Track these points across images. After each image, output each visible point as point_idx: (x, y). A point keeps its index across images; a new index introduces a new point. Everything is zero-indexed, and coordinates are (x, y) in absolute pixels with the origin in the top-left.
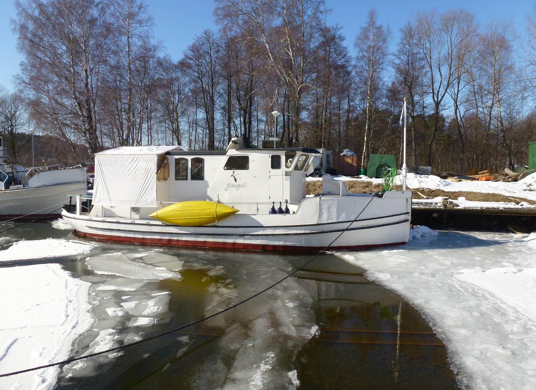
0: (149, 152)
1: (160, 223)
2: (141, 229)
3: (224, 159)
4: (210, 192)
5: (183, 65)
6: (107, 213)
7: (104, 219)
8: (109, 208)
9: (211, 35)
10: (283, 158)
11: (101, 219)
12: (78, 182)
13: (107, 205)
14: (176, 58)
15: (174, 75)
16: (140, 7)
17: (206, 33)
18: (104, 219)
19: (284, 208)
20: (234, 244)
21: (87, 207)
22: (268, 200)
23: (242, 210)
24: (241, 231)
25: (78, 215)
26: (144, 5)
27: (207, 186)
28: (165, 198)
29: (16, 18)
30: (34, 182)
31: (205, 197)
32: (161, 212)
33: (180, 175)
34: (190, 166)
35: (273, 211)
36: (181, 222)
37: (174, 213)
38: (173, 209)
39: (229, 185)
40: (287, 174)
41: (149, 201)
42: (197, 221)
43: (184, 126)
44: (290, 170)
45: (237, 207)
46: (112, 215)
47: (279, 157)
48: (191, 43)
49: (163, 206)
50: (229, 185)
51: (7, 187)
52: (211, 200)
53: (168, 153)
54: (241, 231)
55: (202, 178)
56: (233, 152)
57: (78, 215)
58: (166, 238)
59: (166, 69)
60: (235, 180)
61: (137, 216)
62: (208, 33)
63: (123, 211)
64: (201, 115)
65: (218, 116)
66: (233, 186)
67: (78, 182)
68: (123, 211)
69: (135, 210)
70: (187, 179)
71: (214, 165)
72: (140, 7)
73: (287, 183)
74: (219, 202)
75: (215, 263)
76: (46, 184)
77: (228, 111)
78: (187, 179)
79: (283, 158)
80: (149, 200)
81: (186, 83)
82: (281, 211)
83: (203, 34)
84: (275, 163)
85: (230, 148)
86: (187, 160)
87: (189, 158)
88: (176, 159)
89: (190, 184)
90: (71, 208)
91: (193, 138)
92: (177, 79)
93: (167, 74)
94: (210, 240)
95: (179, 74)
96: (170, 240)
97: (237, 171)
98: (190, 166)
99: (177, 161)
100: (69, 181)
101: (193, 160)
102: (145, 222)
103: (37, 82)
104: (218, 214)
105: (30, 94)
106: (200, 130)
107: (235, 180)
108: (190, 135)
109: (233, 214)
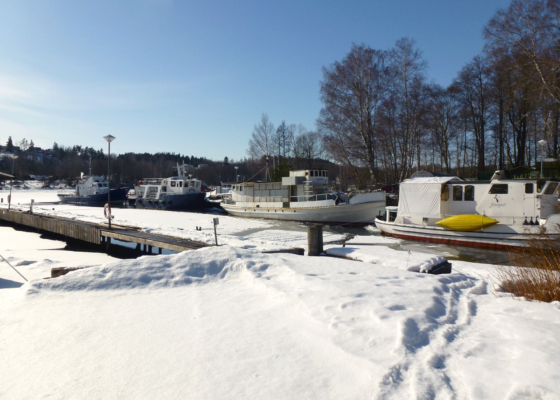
0: (435, 182)
1: (443, 229)
2: (429, 231)
3: (489, 187)
4: (477, 209)
5: (453, 90)
6: (406, 221)
7: (405, 225)
8: (408, 218)
9: (481, 60)
10: (535, 186)
11: (403, 225)
12: (380, 201)
13: (406, 216)
14: (445, 83)
15: (443, 100)
16: (416, 55)
17: (475, 59)
18: (405, 225)
19: (534, 221)
20: (495, 245)
21: (393, 216)
22: (522, 215)
23: (502, 222)
24: (500, 236)
25: (387, 222)
26: (418, 53)
27: (476, 204)
28: (446, 212)
29: (322, 79)
30: (353, 201)
31: (474, 212)
32: (444, 221)
33: (458, 198)
34: (464, 191)
35: (526, 223)
36: (457, 228)
37: (452, 222)
38: (452, 219)
39: (493, 205)
40: (538, 197)
41: (435, 214)
42: (469, 228)
43: (452, 147)
44: (541, 194)
45: (498, 220)
46: (410, 223)
47: (531, 185)
48: (460, 69)
49: (445, 217)
50: (493, 205)
51: (337, 203)
52: (478, 214)
53: (448, 182)
54: (500, 236)
55: (472, 199)
56: (495, 182)
57: (387, 222)
58: (447, 238)
59: (434, 95)
60: (497, 201)
61: (426, 224)
62: (477, 58)
63: (418, 220)
64: (470, 135)
65: (489, 134)
66: (496, 205)
67: (380, 201)
68: (418, 220)
69: (425, 219)
70: (461, 200)
71: (482, 191)
72: (416, 55)
73: (538, 203)
74: (484, 216)
75: (480, 254)
76: (360, 202)
77: (499, 130)
78: (461, 200)
79: (535, 186)
80: (436, 212)
81: (454, 105)
82: (532, 223)
83: (472, 60)
84: (529, 189)
85: (494, 179)
86: (462, 187)
87: (464, 186)
88: (454, 187)
89: (464, 203)
90: (383, 218)
91: (462, 158)
92: (446, 103)
93: (436, 100)
94: (478, 241)
95: (449, 99)
96: (449, 240)
97: (498, 195)
98: (464, 191)
99: (455, 189)
100: (371, 201)
101: (466, 187)
102: (432, 227)
103: (331, 123)
104: (484, 223)
105: (328, 132)
106: (469, 152)
107: (497, 201)
108: (459, 155)
109: (495, 224)
